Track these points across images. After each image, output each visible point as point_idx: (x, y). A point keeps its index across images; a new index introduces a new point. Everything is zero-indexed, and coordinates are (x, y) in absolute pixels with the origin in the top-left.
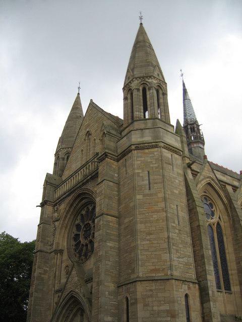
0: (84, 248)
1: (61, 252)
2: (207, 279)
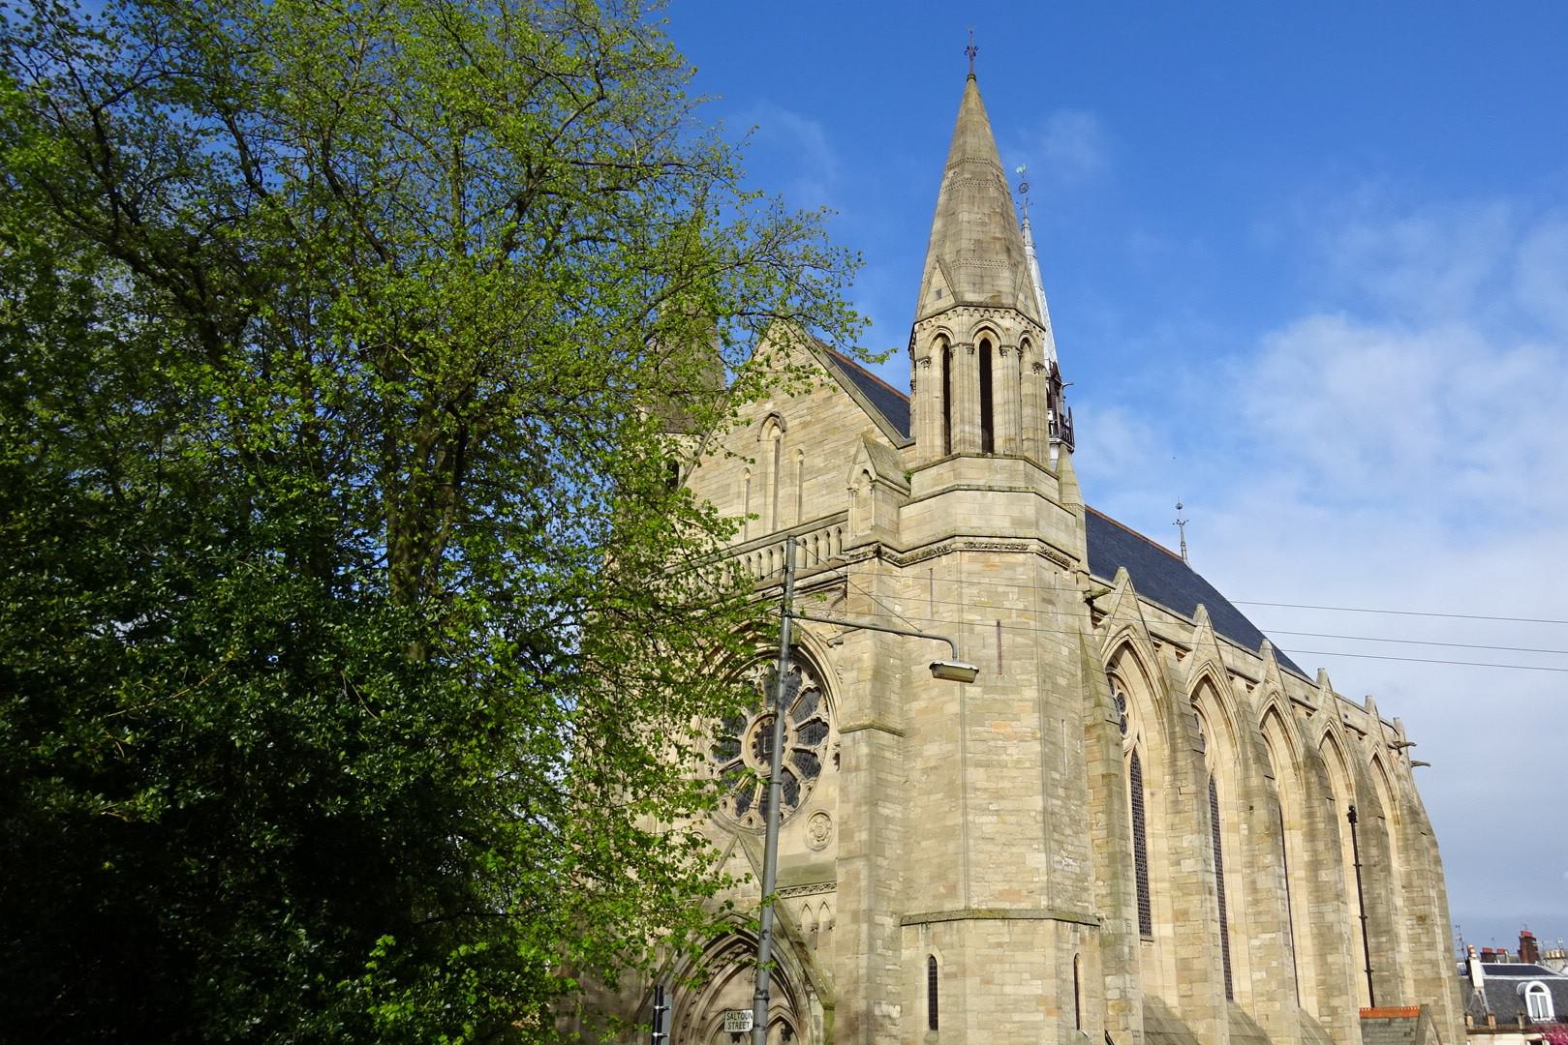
0: (759, 789)
2: (1415, 981)
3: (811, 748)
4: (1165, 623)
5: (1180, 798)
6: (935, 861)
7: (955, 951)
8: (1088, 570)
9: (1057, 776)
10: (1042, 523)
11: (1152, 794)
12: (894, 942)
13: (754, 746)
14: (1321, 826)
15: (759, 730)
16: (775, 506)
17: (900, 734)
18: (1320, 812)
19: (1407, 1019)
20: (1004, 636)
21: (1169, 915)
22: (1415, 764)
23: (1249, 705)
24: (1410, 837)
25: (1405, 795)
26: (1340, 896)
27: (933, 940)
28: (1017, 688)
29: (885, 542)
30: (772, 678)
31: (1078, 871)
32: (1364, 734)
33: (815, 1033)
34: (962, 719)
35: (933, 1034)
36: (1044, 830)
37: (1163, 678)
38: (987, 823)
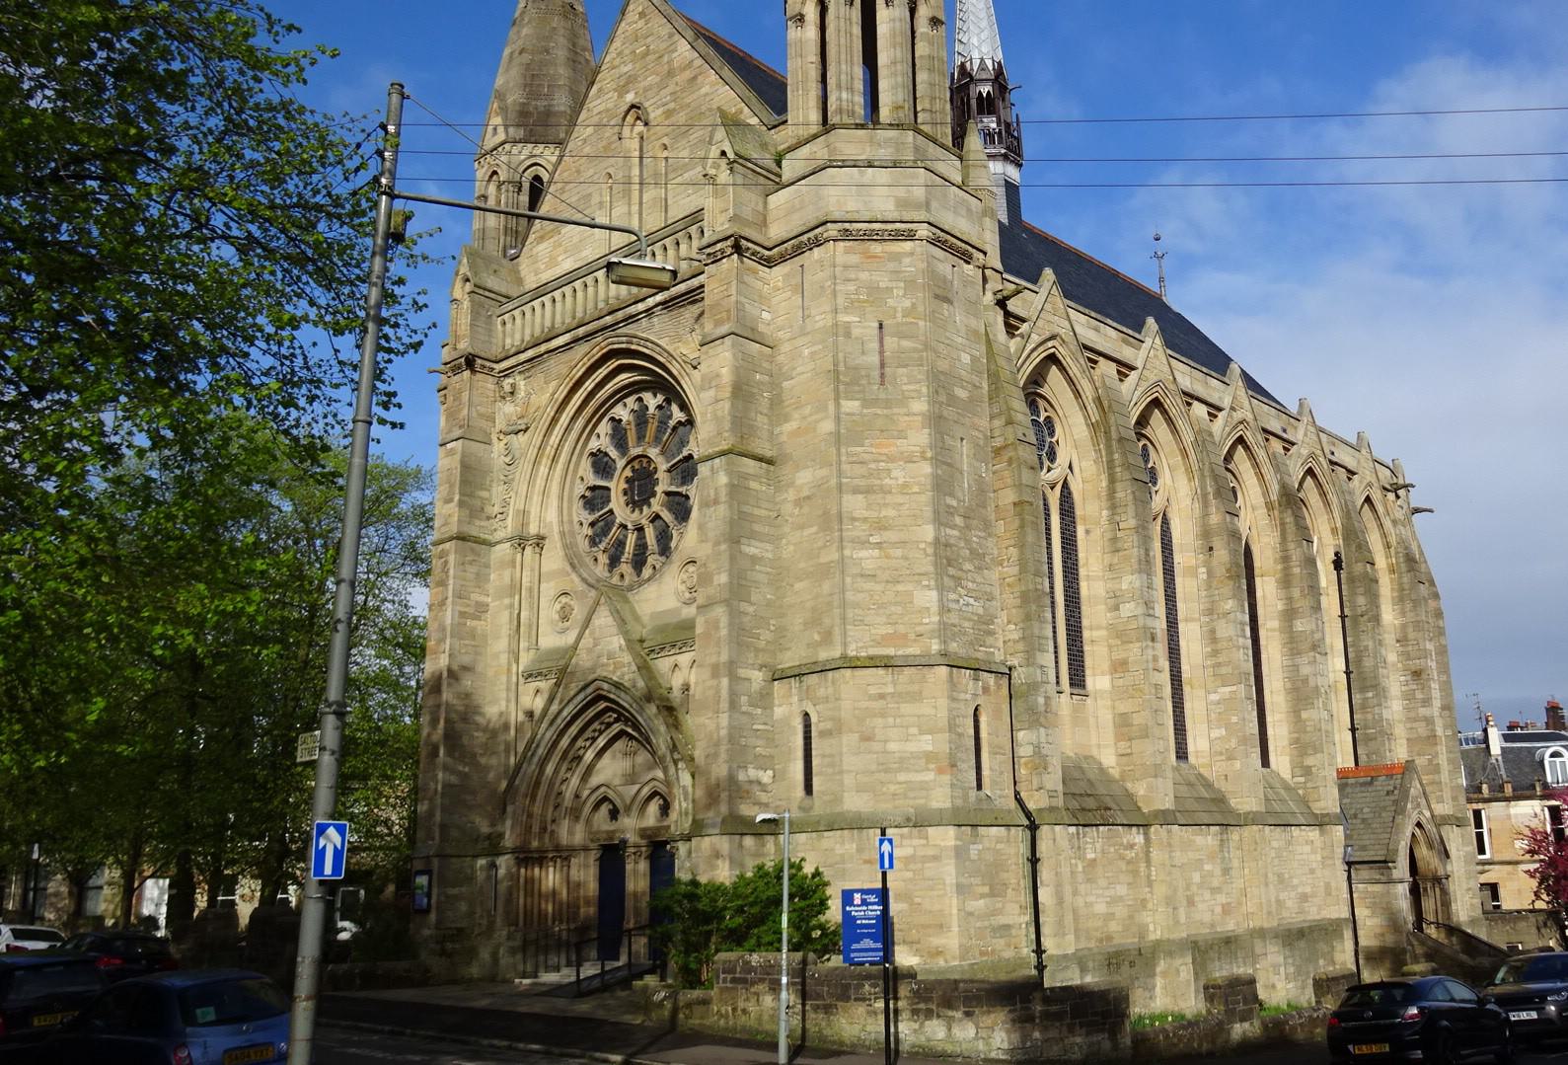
0: (631, 539)
1: (540, 541)
3: (683, 490)
4: (1106, 336)
5: (1119, 534)
6: (809, 605)
7: (830, 706)
8: (999, 266)
9: (954, 503)
10: (934, 205)
11: (1087, 532)
12: (764, 699)
13: (625, 494)
14: (1297, 570)
15: (630, 474)
16: (641, 214)
17: (770, 462)
18: (1296, 555)
19: (1390, 776)
20: (888, 340)
21: (1106, 665)
22: (1417, 511)
23: (1211, 434)
24: (1406, 587)
25: (1402, 541)
26: (1317, 647)
27: (807, 694)
28: (904, 400)
29: (747, 235)
30: (641, 416)
31: (981, 611)
32: (1354, 473)
33: (684, 805)
34: (837, 439)
35: (808, 801)
36: (936, 565)
37: (1099, 398)
38: (868, 558)
